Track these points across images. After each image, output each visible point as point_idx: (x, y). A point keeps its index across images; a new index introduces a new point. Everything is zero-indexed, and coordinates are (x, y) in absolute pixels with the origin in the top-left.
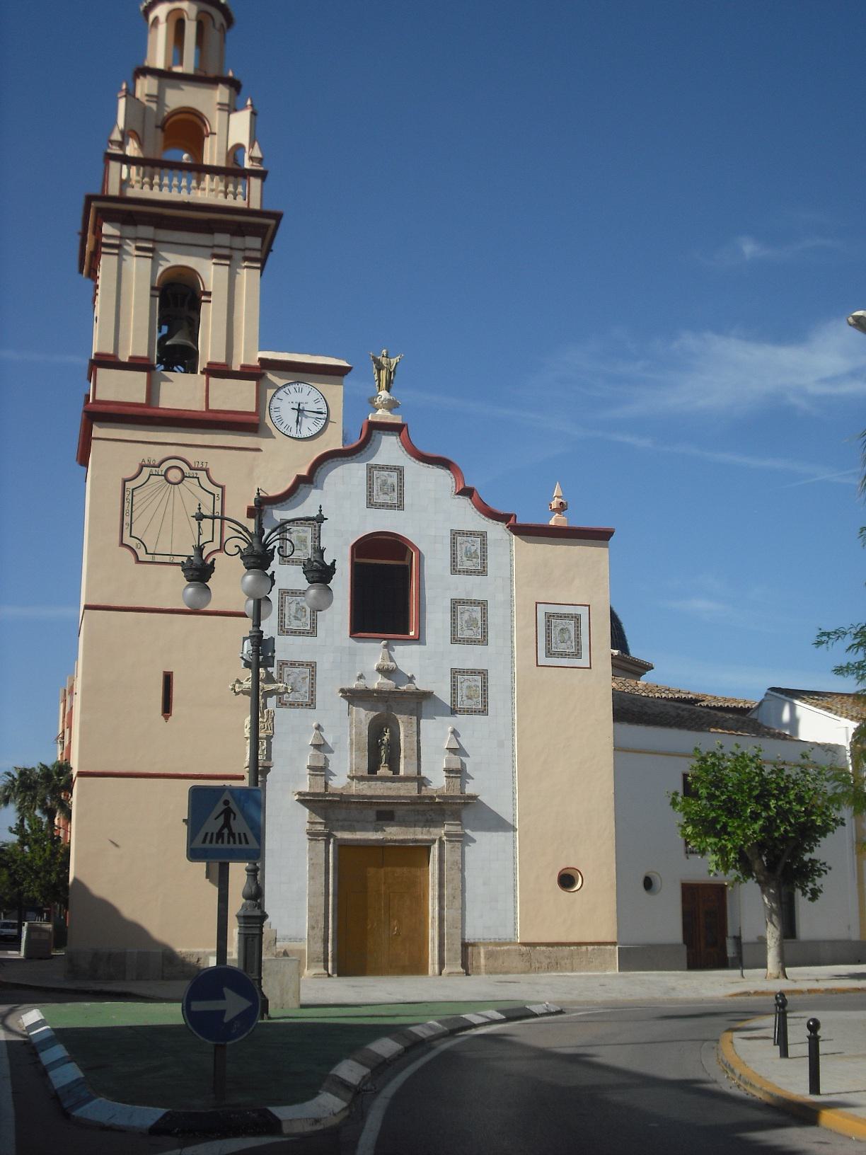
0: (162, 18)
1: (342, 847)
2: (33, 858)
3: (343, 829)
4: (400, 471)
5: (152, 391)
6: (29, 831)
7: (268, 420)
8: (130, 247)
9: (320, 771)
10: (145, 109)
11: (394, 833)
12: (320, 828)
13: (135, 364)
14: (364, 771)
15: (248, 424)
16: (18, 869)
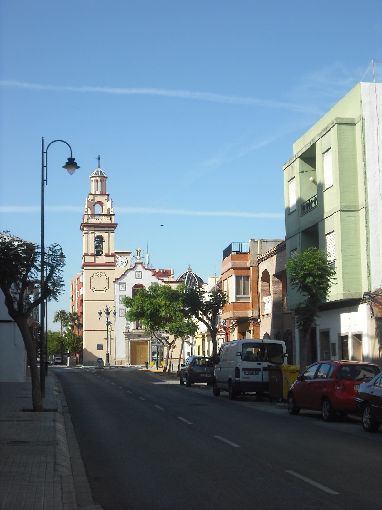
0: (93, 181)
1: (132, 342)
2: (69, 340)
3: (132, 339)
4: (141, 272)
5: (95, 260)
6: (67, 333)
7: (116, 264)
8: (90, 232)
9: (127, 328)
10: (91, 202)
11: (141, 339)
12: (128, 339)
13: (92, 255)
14: (135, 328)
15: (113, 265)
16: (65, 343)
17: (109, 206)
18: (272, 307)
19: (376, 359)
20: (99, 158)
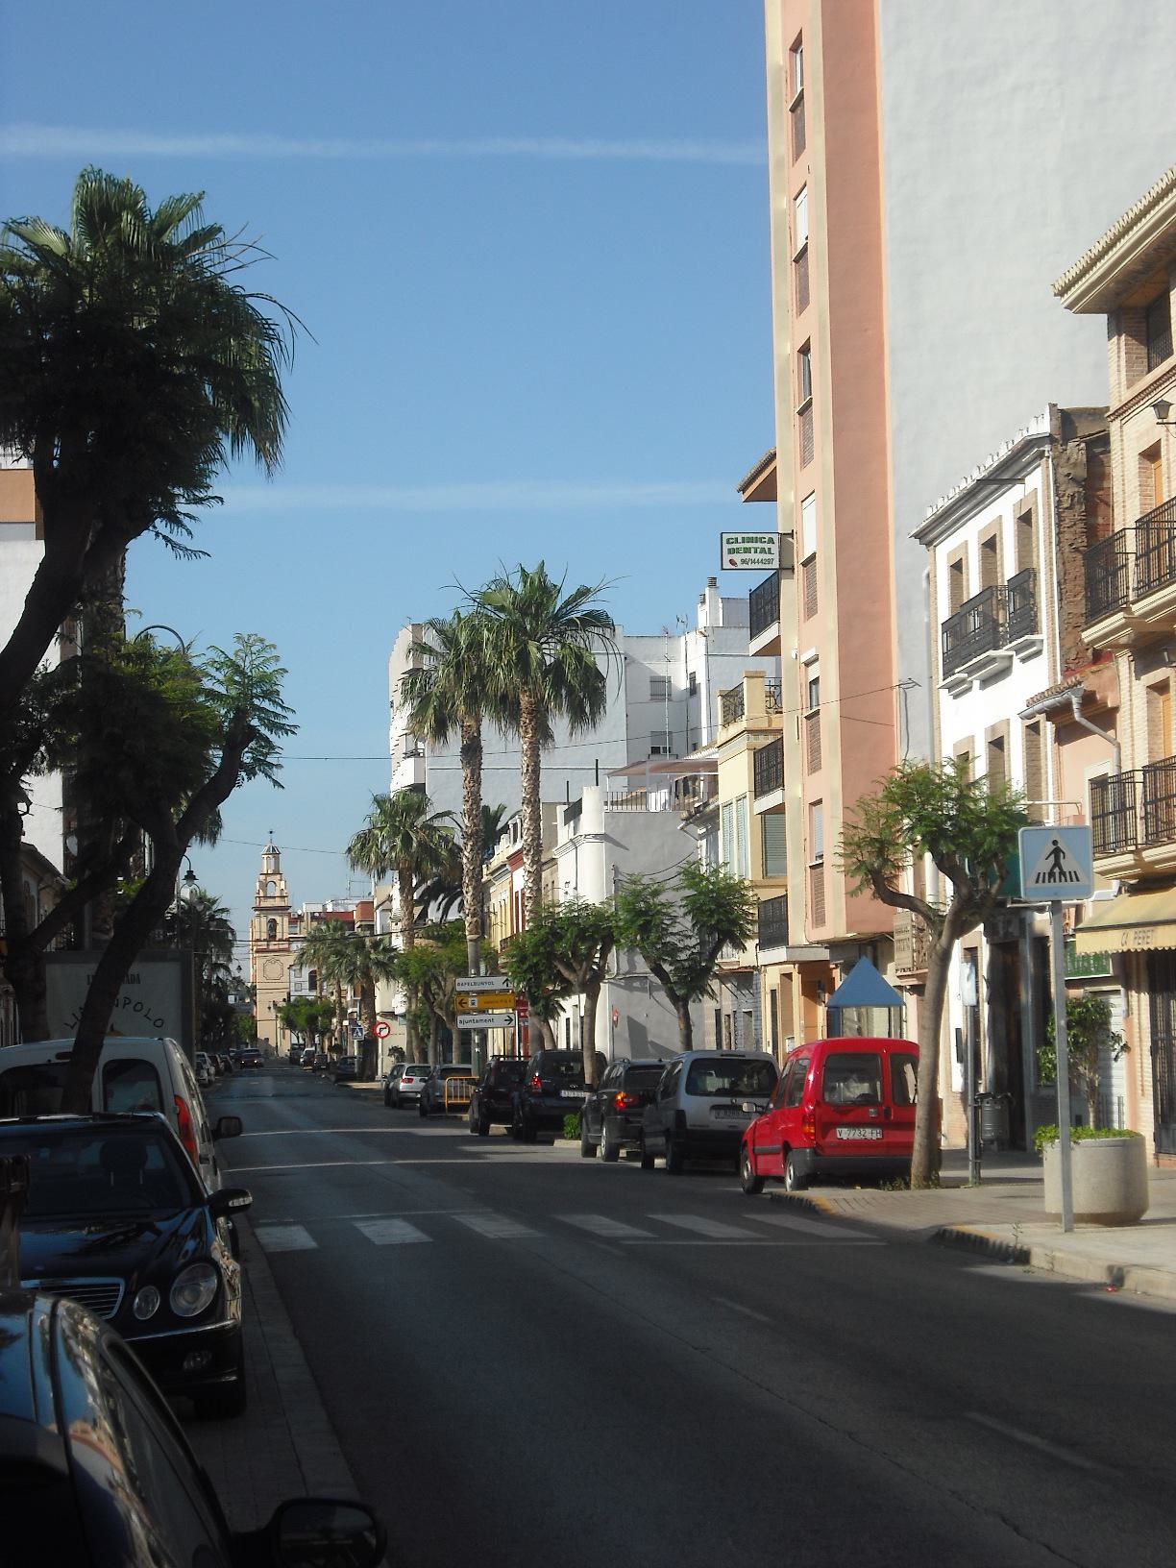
17: (283, 887)
18: (1153, 1307)
19: (1004, 1246)
20: (271, 832)
